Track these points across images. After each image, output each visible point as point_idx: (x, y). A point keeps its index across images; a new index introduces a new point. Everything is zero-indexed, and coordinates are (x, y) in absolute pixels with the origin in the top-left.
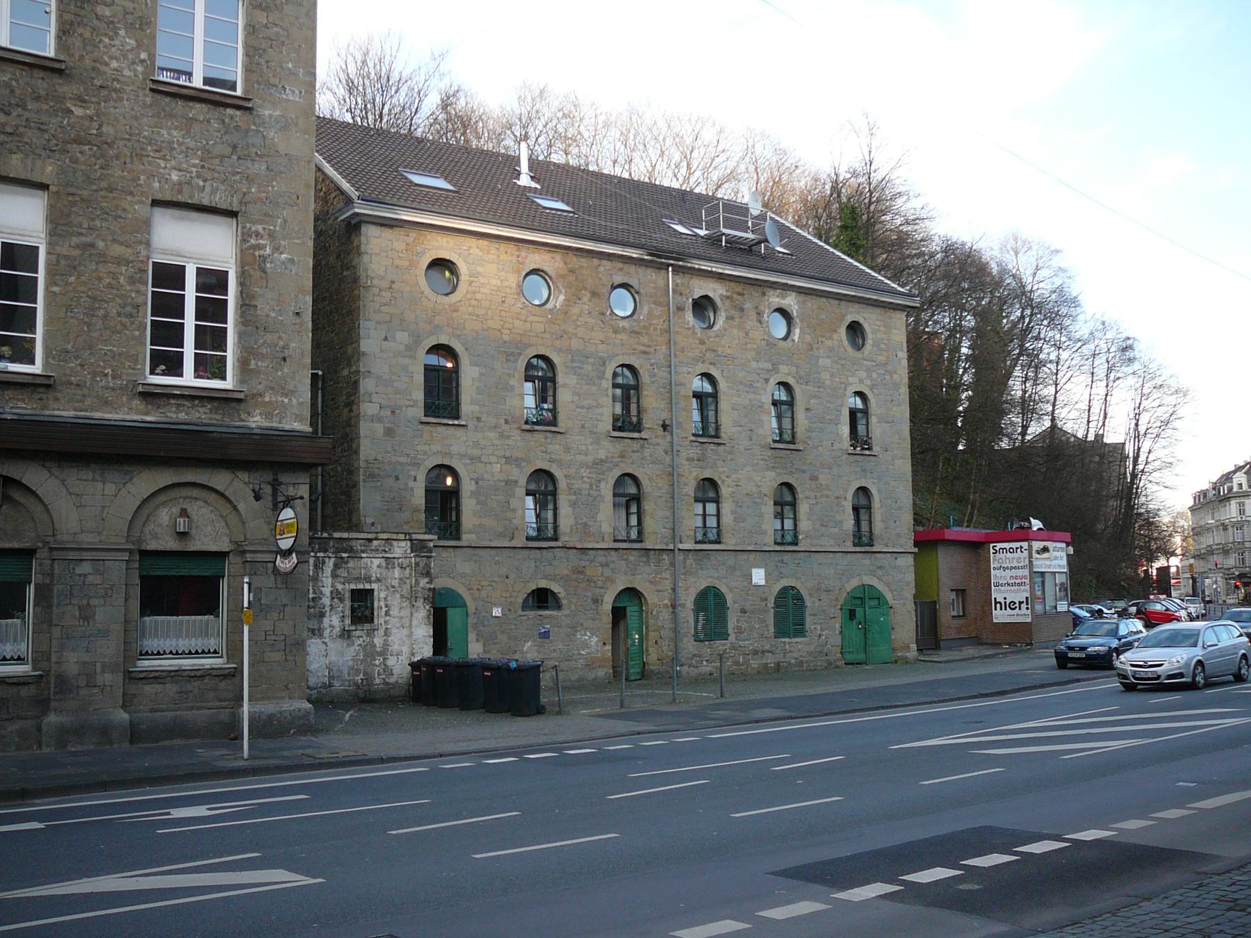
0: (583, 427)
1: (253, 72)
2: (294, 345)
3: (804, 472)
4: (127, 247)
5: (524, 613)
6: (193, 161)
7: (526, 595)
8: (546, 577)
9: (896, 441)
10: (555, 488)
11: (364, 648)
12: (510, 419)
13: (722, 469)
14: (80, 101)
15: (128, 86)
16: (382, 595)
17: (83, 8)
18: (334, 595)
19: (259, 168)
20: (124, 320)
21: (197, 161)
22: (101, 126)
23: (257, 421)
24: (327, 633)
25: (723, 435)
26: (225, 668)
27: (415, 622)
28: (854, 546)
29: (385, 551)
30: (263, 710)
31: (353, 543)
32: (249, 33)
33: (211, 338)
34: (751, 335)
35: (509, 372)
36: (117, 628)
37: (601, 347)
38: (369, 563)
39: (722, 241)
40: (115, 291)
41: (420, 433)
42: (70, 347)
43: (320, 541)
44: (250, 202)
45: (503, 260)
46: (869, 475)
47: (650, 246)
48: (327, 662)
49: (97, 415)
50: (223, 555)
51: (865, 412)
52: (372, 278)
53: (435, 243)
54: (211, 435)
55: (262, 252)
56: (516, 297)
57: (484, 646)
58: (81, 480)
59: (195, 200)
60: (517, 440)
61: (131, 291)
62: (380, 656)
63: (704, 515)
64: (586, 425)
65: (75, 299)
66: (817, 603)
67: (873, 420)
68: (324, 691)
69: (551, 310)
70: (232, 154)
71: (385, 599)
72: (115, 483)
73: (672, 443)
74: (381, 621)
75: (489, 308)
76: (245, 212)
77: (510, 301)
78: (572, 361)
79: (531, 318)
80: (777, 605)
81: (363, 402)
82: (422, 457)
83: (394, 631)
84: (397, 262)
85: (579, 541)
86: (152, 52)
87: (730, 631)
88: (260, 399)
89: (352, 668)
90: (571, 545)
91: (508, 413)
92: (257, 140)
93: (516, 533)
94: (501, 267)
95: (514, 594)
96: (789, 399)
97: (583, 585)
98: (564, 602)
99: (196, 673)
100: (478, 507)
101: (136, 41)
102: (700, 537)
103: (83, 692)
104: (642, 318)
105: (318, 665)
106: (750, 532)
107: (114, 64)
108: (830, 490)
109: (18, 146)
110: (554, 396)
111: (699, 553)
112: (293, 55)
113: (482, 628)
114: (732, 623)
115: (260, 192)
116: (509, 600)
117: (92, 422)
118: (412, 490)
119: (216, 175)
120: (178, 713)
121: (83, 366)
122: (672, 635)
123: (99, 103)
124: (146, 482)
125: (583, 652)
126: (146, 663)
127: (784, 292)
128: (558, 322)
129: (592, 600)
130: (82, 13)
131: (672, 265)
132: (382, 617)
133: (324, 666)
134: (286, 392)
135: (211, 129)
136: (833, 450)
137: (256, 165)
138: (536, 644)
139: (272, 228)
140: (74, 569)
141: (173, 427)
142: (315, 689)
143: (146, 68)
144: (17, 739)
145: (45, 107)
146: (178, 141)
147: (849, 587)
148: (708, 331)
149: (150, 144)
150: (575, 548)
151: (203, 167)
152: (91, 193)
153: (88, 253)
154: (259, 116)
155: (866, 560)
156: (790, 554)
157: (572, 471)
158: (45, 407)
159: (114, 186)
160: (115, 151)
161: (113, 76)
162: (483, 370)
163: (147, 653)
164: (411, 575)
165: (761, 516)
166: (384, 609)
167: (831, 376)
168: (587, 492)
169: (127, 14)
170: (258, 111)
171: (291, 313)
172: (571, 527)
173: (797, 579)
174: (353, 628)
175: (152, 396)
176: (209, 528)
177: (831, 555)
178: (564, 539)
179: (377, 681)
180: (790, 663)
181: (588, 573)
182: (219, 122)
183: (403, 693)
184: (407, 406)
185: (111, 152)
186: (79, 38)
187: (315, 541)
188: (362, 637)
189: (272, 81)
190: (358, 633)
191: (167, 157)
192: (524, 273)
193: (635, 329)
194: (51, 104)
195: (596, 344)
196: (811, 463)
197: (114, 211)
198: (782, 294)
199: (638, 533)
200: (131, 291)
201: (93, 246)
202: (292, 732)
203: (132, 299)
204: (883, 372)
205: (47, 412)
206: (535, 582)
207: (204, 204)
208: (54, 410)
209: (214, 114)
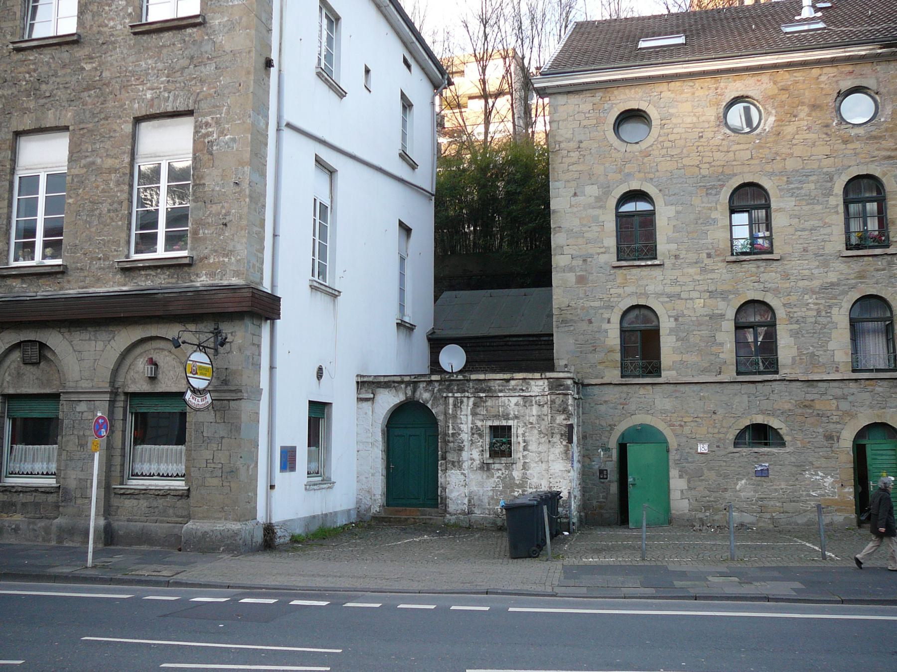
0: (805, 250)
2: (233, 211)
4: (116, 158)
7: (739, 431)
8: (762, 412)
11: (503, 480)
12: (712, 252)
14: (90, 59)
15: (120, 36)
16: (520, 431)
18: (474, 431)
21: (165, 78)
22: (101, 73)
23: (203, 281)
24: (466, 465)
27: (552, 457)
35: (710, 205)
37: (825, 162)
38: (506, 401)
40: (106, 194)
41: (612, 277)
43: (458, 382)
44: (202, 100)
49: (91, 290)
52: (560, 142)
55: (210, 138)
57: (689, 482)
58: (82, 340)
59: (162, 110)
60: (722, 273)
62: (519, 488)
65: (82, 205)
68: (462, 517)
70: (190, 65)
71: (523, 435)
72: (103, 341)
75: (685, 146)
77: (708, 134)
78: (789, 182)
81: (555, 255)
83: (533, 465)
84: (584, 123)
89: (492, 498)
92: (208, 47)
93: (723, 367)
94: (696, 104)
98: (787, 438)
99: (159, 492)
103: (79, 501)
104: (882, 120)
105: (458, 494)
107: (112, 24)
109: (52, 104)
115: (209, 89)
116: (717, 436)
118: (606, 331)
120: (145, 524)
121: (86, 254)
124: (126, 337)
126: (134, 482)
128: (768, 145)
129: (825, 436)
133: (463, 495)
137: (208, 67)
139: (218, 116)
140: (75, 407)
142: (455, 514)
144: (43, 533)
145: (69, 71)
149: (133, 76)
150: (798, 380)
151: (168, 81)
153: (91, 169)
157: (793, 298)
159: (108, 115)
162: (680, 208)
166: (522, 444)
168: (813, 320)
170: (210, 23)
171: (232, 184)
172: (793, 358)
174: (491, 461)
175: (129, 270)
176: (171, 372)
178: (784, 372)
181: (817, 407)
184: (599, 254)
186: (90, 13)
188: (501, 470)
190: (497, 466)
193: (873, 133)
194: (72, 67)
195: (820, 160)
201: (93, 163)
203: (118, 197)
205: (62, 292)
206: (750, 417)
208: (67, 290)
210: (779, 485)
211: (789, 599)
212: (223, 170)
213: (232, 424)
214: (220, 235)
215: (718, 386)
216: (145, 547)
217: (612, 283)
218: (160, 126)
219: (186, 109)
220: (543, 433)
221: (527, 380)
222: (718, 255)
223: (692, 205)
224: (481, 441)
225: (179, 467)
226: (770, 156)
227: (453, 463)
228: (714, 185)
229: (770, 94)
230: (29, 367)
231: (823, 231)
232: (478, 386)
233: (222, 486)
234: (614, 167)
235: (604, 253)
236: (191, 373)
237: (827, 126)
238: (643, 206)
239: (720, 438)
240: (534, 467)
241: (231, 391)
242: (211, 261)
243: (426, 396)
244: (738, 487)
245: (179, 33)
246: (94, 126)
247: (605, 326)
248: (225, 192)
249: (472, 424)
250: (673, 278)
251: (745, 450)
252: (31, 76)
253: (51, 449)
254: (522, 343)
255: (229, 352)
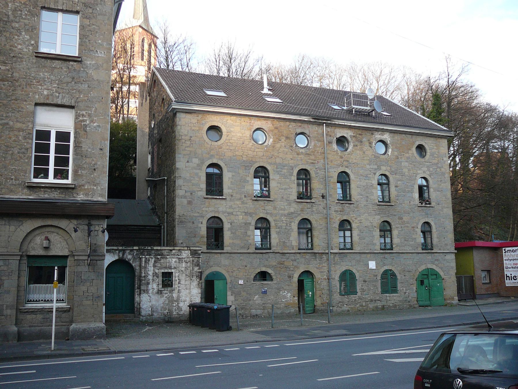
0: (282, 198)
1: (83, 45)
2: (99, 163)
3: (395, 215)
4: (23, 124)
5: (254, 283)
6: (54, 85)
7: (255, 274)
8: (265, 266)
9: (443, 200)
10: (270, 226)
11: (168, 298)
12: (247, 195)
13: (352, 215)
14: (4, 63)
16: (177, 275)
17: (6, 25)
18: (154, 275)
19: (85, 86)
20: (21, 155)
21: (56, 85)
22: (13, 73)
23: (81, 197)
24: (150, 291)
25: (352, 199)
26: (65, 308)
27: (192, 287)
28: (422, 250)
29: (178, 255)
30: (80, 327)
31: (163, 252)
32: (81, 29)
33: (62, 162)
34: (366, 153)
36: (14, 290)
37: (291, 162)
39: (353, 111)
40: (17, 143)
45: (243, 125)
46: (429, 216)
47: (315, 115)
48: (151, 304)
49: (7, 196)
51: (427, 186)
52: (181, 136)
53: (210, 119)
54: (57, 204)
55: (85, 123)
56: (250, 141)
60: (250, 204)
61: (25, 142)
63: (344, 237)
64: (284, 197)
66: (404, 277)
67: (431, 190)
68: (149, 317)
69: (266, 146)
70: (72, 81)
71: (178, 276)
72: (15, 226)
73: (327, 204)
74: (176, 286)
75: (237, 146)
76: (78, 106)
77: (246, 142)
78: (277, 168)
79: (256, 150)
80: (382, 278)
81: (178, 190)
82: (205, 213)
83: (182, 291)
84: (193, 128)
85: (281, 250)
86: (37, 41)
87: (358, 290)
88: (83, 188)
89: (163, 307)
90: (277, 251)
91: (246, 192)
92: (84, 75)
94: (242, 128)
95: (249, 274)
96: (388, 182)
97: (283, 270)
98: (274, 277)
100: (232, 235)
101: (30, 36)
102: (342, 247)
104: (311, 147)
105: (146, 306)
106: (368, 244)
107: (20, 47)
108: (409, 224)
110: (269, 184)
111: (341, 254)
112: (101, 37)
113: (234, 289)
114: (359, 287)
117: (5, 199)
119: (65, 91)
120: (42, 328)
122: (328, 292)
123: (12, 64)
124: (29, 225)
125: (283, 300)
126: (30, 305)
127: (383, 133)
128: (270, 151)
130: (6, 26)
131: (325, 123)
132: (177, 284)
133: (149, 306)
134: (95, 184)
135: (63, 71)
136: (410, 205)
137: (83, 85)
138: (260, 296)
139: (90, 112)
141: (42, 201)
143: (34, 47)
146: (47, 77)
147: (420, 270)
148: (344, 152)
149: (35, 79)
150: (279, 253)
151: (58, 88)
152: (7, 102)
153: (5, 127)
154: (85, 64)
155: (429, 257)
156: (388, 254)
157: (278, 218)
160: (19, 83)
161: (19, 52)
163: (31, 301)
164: (190, 265)
165: (373, 236)
166: (178, 281)
167: (409, 170)
168: (285, 227)
169: (26, 25)
170: (84, 62)
171: (98, 149)
172: (277, 243)
173: (392, 266)
175: (32, 187)
176: (59, 245)
177: (410, 254)
178: (273, 249)
179: (174, 313)
180: (389, 306)
181: (285, 264)
182: (67, 68)
183: (186, 319)
184: (198, 191)
185: (17, 84)
187: (145, 251)
188: (167, 293)
189: (91, 48)
190: (165, 292)
191: (43, 84)
192: (253, 130)
195: (289, 160)
196: (398, 212)
197: (18, 109)
198: (382, 133)
199: (311, 246)
200: (25, 142)
201: (8, 124)
202: (94, 337)
203: (25, 146)
204: (436, 167)
206: (260, 268)
207: (58, 103)
209: (64, 65)
210: (271, 298)
213: (99, 272)
214: (91, 174)
215: (248, 254)
216: (42, 340)
217: (204, 205)
219: (70, 105)
220: (187, 276)
221: (180, 251)
222: (249, 197)
223: (238, 173)
224: (158, 279)
225: (58, 296)
226: (271, 156)
227: (144, 290)
228: (248, 165)
229: (271, 129)
231: (289, 190)
232: (157, 253)
233: (93, 304)
234: (206, 151)
235: (200, 191)
237: (292, 147)
238: (216, 171)
239: (248, 278)
240: (183, 292)
241: (98, 255)
242: (86, 187)
243: (130, 257)
244: (255, 299)
245: (65, 63)
246: (7, 102)
247: (200, 225)
248: (94, 153)
249: (153, 271)
250: (230, 205)
251: (258, 282)
254: (136, 229)
255: (97, 236)
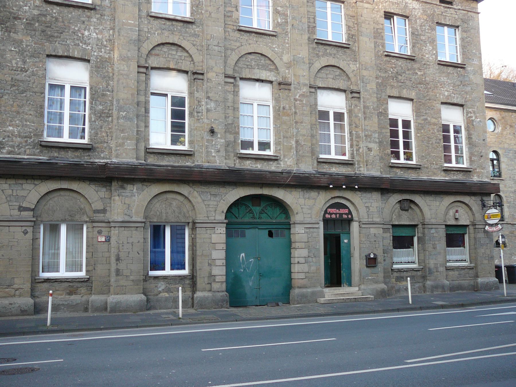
19: (468, 89)
22: (425, 77)
42: (424, 154)
49: (433, 178)
50: (467, 226)
55: (472, 119)
78: (505, 152)
98: (507, 244)
103: (435, 274)
107: (427, 56)
115: (470, 97)
145: (411, 73)
149: (439, 83)
151: (453, 89)
158: (419, 176)
175: (447, 171)
201: (427, 119)
211: (393, 309)
212: (478, 133)
218: (447, 108)
230: (404, 212)
236: (488, 218)
252: (394, 70)
253: (79, 258)
